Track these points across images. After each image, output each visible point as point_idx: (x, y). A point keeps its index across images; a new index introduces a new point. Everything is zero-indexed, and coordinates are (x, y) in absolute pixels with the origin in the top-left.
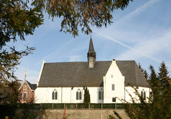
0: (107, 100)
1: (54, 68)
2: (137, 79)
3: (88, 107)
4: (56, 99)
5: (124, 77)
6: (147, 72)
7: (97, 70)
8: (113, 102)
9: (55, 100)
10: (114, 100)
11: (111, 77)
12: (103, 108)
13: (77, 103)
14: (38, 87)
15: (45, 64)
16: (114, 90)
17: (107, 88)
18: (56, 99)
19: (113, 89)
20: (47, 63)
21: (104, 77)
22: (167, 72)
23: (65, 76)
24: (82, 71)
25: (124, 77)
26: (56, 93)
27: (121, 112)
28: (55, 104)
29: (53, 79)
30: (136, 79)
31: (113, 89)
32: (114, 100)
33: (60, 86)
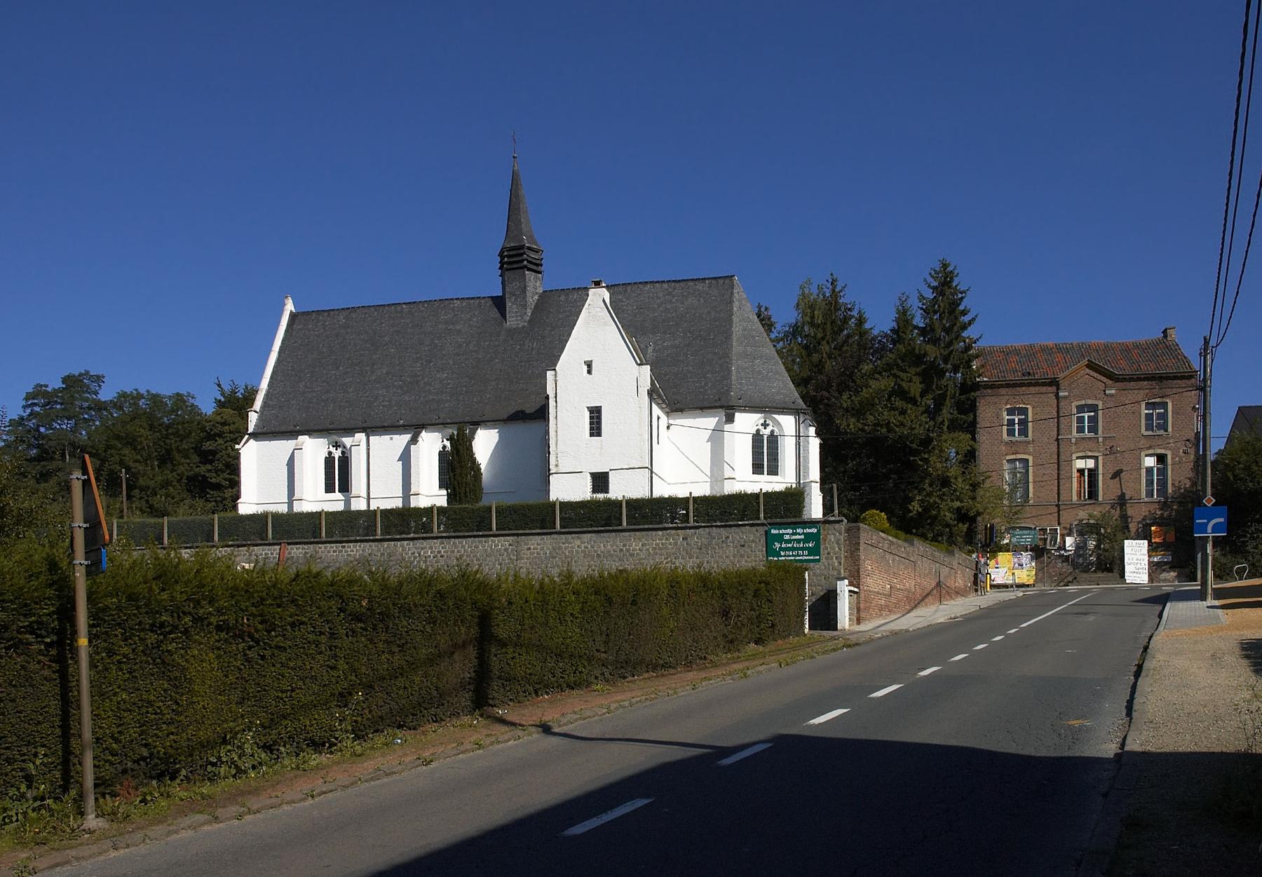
0: (569, 487)
1: (337, 335)
2: (734, 373)
3: (554, 523)
4: (774, 471)
5: (647, 369)
6: (867, 326)
7: (543, 337)
8: (594, 492)
9: (765, 477)
10: (600, 481)
11: (585, 368)
12: (561, 527)
13: (561, 503)
14: (255, 436)
15: (293, 316)
16: (599, 435)
17: (566, 424)
18: (774, 471)
19: (596, 429)
20: (303, 313)
21: (550, 374)
22: (966, 319)
23: (387, 373)
24: (471, 346)
25: (647, 369)
26: (773, 439)
27: (578, 542)
28: (768, 495)
29: (328, 392)
30: (729, 371)
31: (596, 429)
32: (600, 481)
33: (360, 424)
